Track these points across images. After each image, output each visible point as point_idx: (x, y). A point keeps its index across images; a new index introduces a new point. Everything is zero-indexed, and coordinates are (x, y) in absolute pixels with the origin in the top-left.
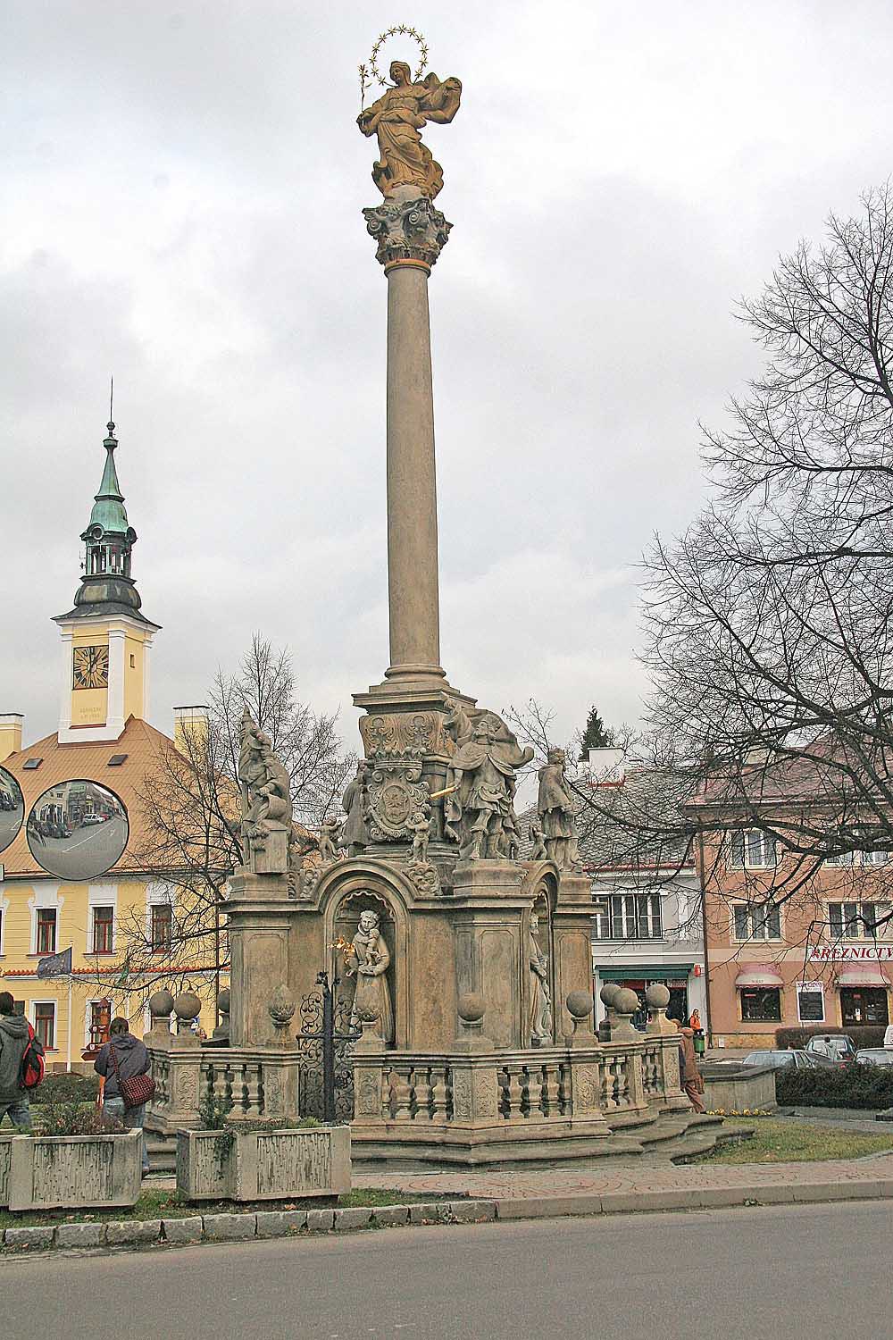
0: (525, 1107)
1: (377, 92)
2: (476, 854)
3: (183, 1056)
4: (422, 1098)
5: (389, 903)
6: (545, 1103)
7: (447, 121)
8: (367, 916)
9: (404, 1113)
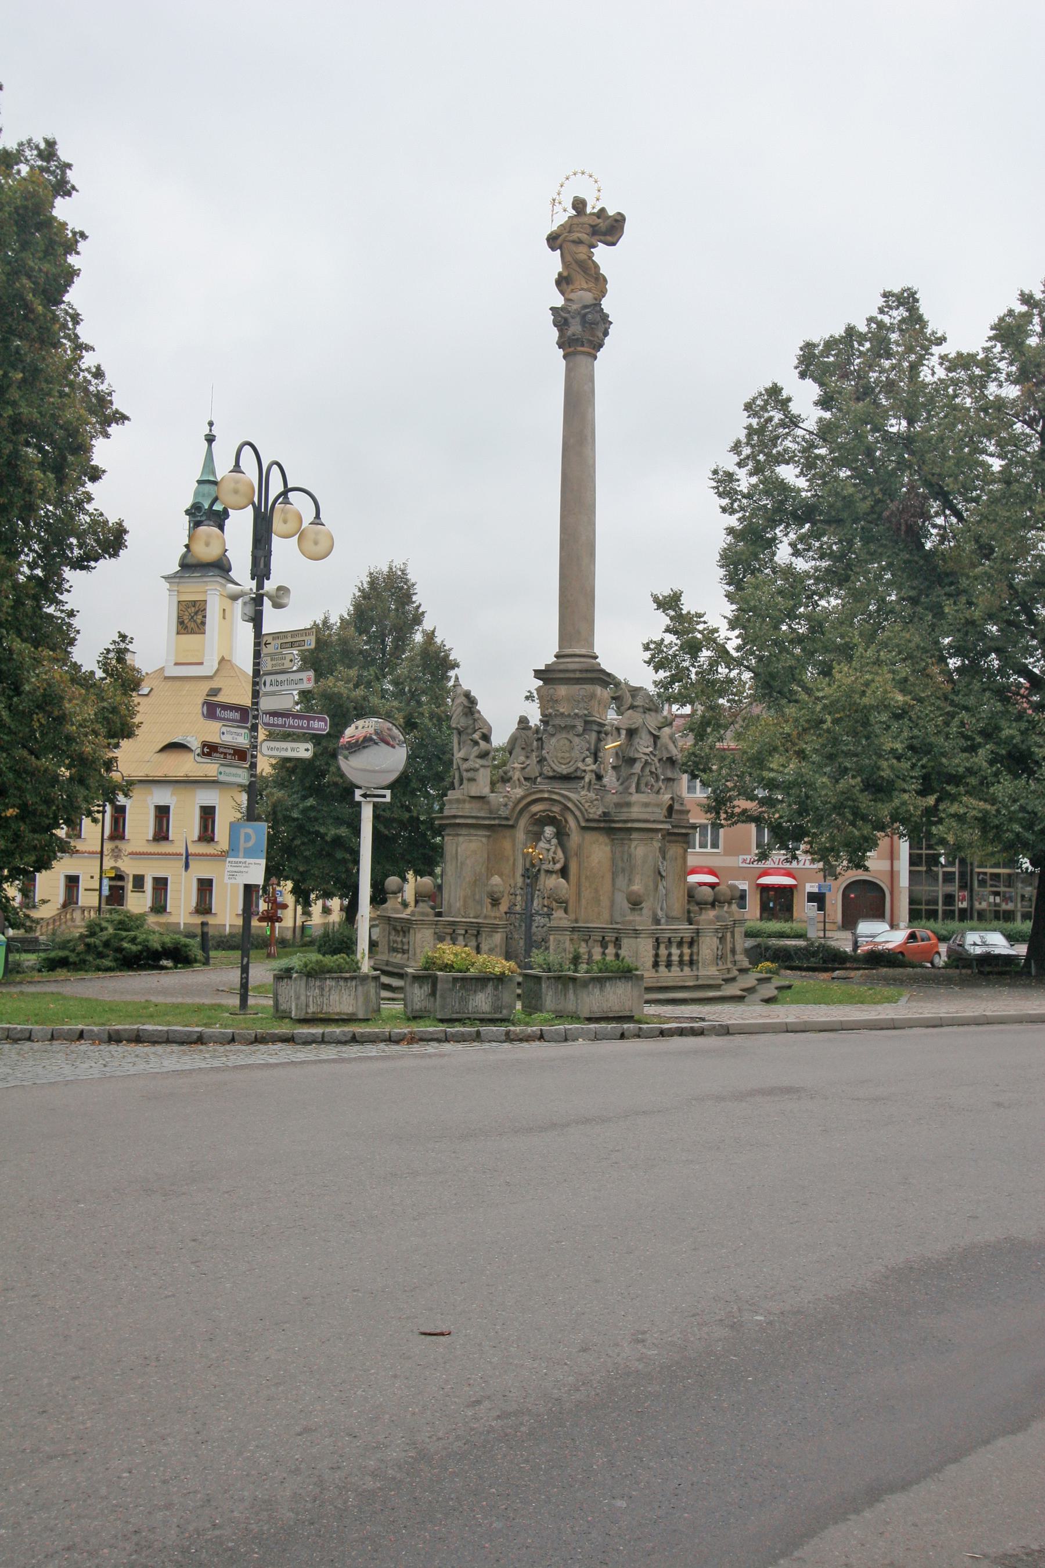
0: (669, 965)
1: (562, 218)
2: (633, 789)
5: (566, 821)
6: (681, 963)
7: (614, 244)
8: (549, 831)
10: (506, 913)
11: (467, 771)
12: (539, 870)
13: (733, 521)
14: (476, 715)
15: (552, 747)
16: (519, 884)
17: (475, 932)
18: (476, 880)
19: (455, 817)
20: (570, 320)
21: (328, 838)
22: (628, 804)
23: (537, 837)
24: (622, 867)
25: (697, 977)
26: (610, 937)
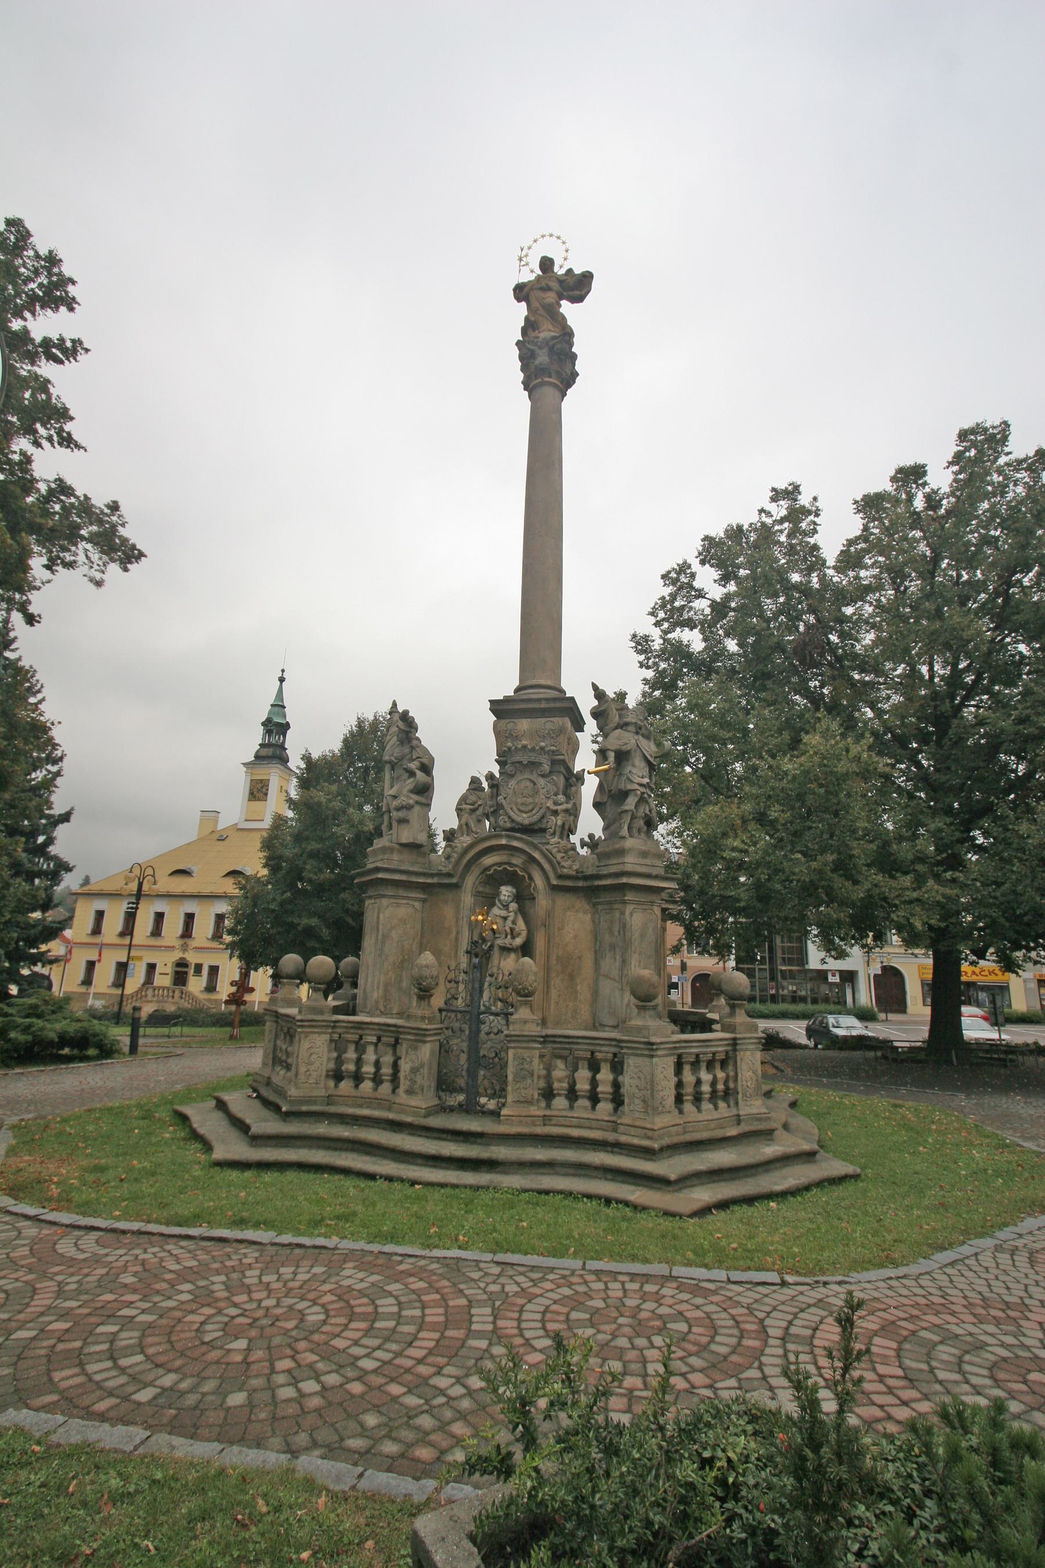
2: (625, 832)
3: (312, 1024)
4: (583, 1086)
5: (531, 878)
6: (714, 1096)
8: (506, 892)
9: (560, 1102)
10: (440, 1010)
11: (398, 809)
12: (492, 946)
13: (650, 674)
14: (415, 742)
15: (510, 792)
16: (464, 965)
17: (392, 1040)
18: (402, 962)
19: (378, 870)
20: (538, 351)
21: (300, 928)
22: (621, 852)
23: (489, 900)
24: (608, 943)
25: (738, 1120)
26: (604, 1053)
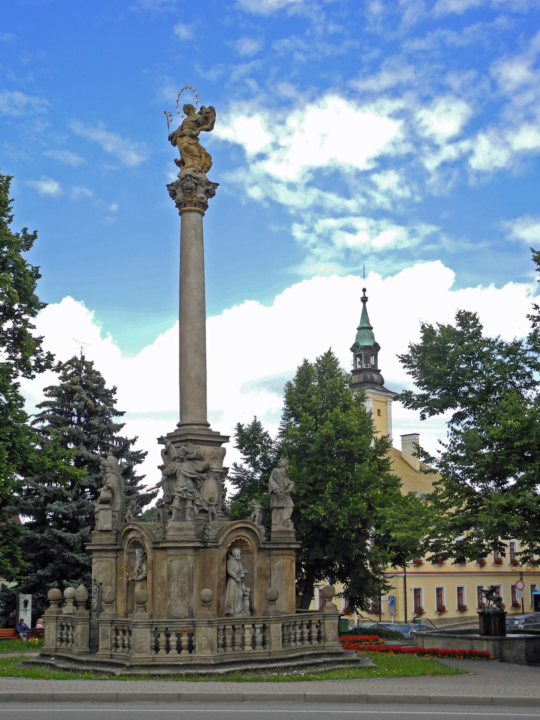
25: (192, 659)
